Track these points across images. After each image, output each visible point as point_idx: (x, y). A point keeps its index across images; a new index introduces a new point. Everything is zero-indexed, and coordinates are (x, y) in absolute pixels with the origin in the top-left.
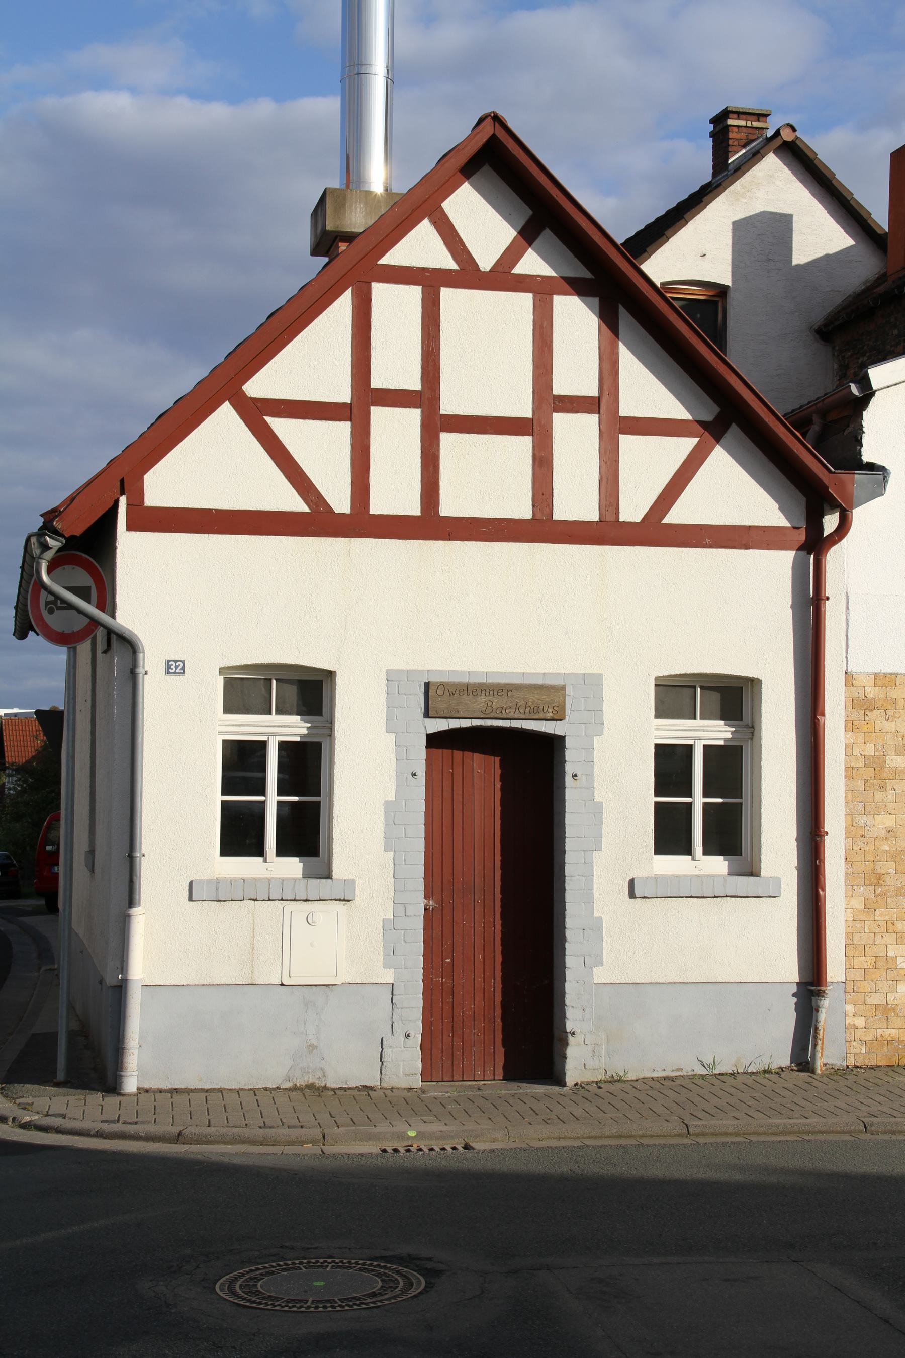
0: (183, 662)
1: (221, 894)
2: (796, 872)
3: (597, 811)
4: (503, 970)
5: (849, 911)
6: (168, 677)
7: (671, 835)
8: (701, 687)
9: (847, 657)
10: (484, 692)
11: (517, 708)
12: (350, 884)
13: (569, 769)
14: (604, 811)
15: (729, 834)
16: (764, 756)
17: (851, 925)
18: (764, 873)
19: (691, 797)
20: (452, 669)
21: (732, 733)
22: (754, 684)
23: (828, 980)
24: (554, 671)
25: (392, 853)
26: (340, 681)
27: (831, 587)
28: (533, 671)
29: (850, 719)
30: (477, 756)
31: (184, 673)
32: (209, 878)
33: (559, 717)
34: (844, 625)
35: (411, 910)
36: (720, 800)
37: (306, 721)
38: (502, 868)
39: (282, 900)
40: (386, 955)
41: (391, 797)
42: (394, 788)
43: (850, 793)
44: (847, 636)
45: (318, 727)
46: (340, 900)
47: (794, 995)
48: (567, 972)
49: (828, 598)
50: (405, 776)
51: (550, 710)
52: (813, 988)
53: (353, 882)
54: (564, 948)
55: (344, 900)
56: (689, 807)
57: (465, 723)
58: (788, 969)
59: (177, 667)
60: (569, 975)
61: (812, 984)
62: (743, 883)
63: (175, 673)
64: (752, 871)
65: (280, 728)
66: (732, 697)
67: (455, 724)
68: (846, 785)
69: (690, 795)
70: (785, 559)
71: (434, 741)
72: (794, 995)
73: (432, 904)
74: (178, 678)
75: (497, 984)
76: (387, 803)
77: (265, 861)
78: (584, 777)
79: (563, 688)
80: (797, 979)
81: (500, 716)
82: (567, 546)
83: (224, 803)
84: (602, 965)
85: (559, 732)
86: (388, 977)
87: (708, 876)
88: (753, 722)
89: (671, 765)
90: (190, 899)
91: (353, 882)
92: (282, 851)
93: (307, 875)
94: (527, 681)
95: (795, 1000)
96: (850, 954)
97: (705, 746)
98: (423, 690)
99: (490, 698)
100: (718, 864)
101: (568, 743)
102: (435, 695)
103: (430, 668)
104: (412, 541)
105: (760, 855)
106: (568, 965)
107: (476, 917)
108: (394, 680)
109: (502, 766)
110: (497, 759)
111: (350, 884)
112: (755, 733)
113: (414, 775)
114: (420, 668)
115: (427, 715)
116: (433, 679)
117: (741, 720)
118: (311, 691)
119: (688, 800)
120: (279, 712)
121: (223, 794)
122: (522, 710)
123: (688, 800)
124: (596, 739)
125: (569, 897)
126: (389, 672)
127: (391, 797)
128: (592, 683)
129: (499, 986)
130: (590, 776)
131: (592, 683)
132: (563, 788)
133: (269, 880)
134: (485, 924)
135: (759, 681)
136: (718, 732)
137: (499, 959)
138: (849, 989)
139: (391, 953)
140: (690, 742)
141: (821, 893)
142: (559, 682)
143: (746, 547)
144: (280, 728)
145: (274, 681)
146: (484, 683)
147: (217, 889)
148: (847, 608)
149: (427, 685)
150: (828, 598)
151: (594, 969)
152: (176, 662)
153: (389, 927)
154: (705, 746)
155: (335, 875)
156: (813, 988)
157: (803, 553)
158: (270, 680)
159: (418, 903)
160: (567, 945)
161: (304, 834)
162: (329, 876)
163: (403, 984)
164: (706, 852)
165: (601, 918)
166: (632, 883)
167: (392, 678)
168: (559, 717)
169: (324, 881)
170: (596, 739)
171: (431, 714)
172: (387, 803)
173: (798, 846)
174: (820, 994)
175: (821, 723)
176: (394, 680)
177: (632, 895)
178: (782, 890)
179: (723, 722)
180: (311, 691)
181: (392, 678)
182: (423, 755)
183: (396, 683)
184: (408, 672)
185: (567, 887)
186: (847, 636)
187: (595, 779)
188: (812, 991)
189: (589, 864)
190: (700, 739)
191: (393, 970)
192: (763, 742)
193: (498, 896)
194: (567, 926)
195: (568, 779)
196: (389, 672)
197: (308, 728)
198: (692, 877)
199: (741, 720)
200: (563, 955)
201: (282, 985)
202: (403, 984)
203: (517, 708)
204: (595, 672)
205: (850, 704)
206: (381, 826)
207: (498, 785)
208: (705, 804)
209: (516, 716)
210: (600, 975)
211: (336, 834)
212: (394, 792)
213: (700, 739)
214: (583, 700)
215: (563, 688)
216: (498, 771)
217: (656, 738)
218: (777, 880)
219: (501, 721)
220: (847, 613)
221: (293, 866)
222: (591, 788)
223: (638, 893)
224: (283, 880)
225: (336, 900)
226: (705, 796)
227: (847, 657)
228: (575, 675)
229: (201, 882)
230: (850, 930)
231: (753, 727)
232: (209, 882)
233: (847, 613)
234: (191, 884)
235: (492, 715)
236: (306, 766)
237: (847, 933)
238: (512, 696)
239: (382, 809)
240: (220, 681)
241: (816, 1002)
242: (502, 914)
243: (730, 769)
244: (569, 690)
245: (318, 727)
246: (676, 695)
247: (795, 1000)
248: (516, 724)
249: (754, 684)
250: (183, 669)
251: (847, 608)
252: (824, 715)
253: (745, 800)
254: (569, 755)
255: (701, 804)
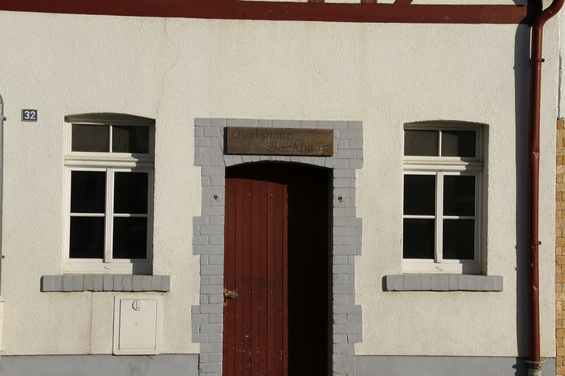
0: (36, 111)
1: (65, 285)
2: (515, 273)
3: (358, 225)
4: (289, 344)
5: (559, 303)
6: (25, 123)
7: (417, 243)
8: (443, 132)
9: (559, 107)
10: (269, 135)
11: (296, 147)
12: (166, 279)
13: (336, 193)
14: (364, 225)
15: (465, 243)
16: (490, 184)
17: (560, 313)
18: (489, 273)
19: (434, 215)
20: (245, 118)
21: (466, 166)
22: (483, 128)
23: (542, 355)
24: (325, 119)
25: (199, 256)
26: (158, 126)
27: (545, 53)
28: (309, 120)
29: (561, 154)
30: (270, 184)
31: (36, 120)
32: (57, 274)
33: (328, 153)
34: (557, 81)
35: (213, 299)
36: (128, 215)
37: (135, 157)
38: (289, 267)
39: (113, 291)
40: (194, 332)
41: (199, 214)
42: (200, 207)
43: (560, 212)
44: (559, 90)
45: (144, 162)
46: (158, 291)
47: (514, 367)
48: (334, 347)
49: (543, 60)
50: (208, 198)
51: (321, 149)
52: (529, 362)
53: (168, 277)
54: (332, 329)
55: (161, 291)
56: (432, 222)
57: (256, 159)
58: (510, 347)
59: (31, 115)
60: (336, 349)
61: (528, 359)
62: (473, 280)
63: (29, 120)
64: (482, 272)
65: (115, 162)
66: (467, 139)
67: (248, 159)
68: (557, 206)
69: (103, 211)
70: (509, 31)
71: (232, 173)
72: (514, 367)
73: (232, 293)
74: (32, 123)
75: (284, 354)
76: (195, 219)
77: (104, 262)
78: (348, 199)
79: (331, 132)
80: (516, 354)
81: (282, 153)
82: (336, 23)
83: (72, 218)
84: (361, 341)
85: (328, 165)
86: (196, 349)
87: (446, 274)
88: (483, 157)
89: (417, 191)
90: (42, 290)
91: (168, 277)
92: (117, 254)
93: (136, 272)
94: (303, 127)
95: (515, 370)
96: (560, 335)
97: (445, 176)
98: (223, 134)
99: (275, 140)
100: (455, 266)
101: (336, 173)
102: (235, 137)
103: (229, 117)
104: (214, 20)
105: (486, 259)
106: (334, 341)
107: (269, 304)
108: (201, 126)
109: (289, 191)
110: (285, 187)
111: (166, 279)
112: (485, 166)
113: (216, 197)
114: (221, 117)
115: (226, 152)
116: (230, 125)
117: (474, 156)
118: (136, 134)
119: (432, 217)
120: (115, 150)
121: (405, 214)
122: (299, 149)
123: (432, 217)
124: (357, 171)
125: (336, 289)
126: (196, 120)
127: (199, 214)
128: (355, 129)
129: (286, 356)
130: (352, 199)
131: (355, 129)
132: (332, 207)
133: (103, 276)
134: (276, 309)
135: (488, 126)
136: (456, 165)
137: (286, 335)
138: (560, 363)
139: (198, 333)
140: (434, 173)
141: (535, 288)
142: (329, 127)
143: (478, 21)
144: (115, 162)
145: (111, 127)
146: (269, 128)
147: (62, 283)
148: (560, 68)
149: (226, 130)
150: (543, 60)
151: (355, 345)
152: (30, 111)
153: (196, 311)
154: (445, 176)
155: (155, 273)
156: (529, 362)
157: (524, 26)
158: (108, 127)
159: (218, 292)
160: (334, 326)
161: (135, 242)
162: (151, 274)
163: (207, 355)
164: (445, 257)
165: (360, 306)
166: (384, 279)
167: (199, 124)
168: (328, 153)
169: (145, 277)
170: (357, 171)
171: (228, 151)
172: (195, 219)
173: (517, 253)
174: (535, 367)
175: (536, 157)
176: (201, 126)
177: (385, 289)
178: (504, 286)
179: (459, 158)
180: (136, 134)
181: (199, 124)
182: (223, 183)
183: (202, 128)
184: (211, 120)
185: (334, 282)
186: (559, 90)
187: (357, 201)
188: (528, 364)
189: (351, 265)
190: (441, 171)
191: (199, 344)
192: (490, 173)
193: (286, 288)
194: (334, 312)
195: (336, 202)
196: (196, 120)
197: (137, 163)
198: (431, 276)
199: (474, 156)
200: (332, 334)
201: (113, 355)
202: (207, 355)
203: (296, 147)
204: (357, 120)
205: (561, 143)
206: (190, 235)
207: (286, 206)
208: (445, 220)
209: (294, 153)
210: (360, 349)
211: (155, 243)
212: (200, 210)
213: (441, 171)
214: (347, 141)
215: (331, 132)
216: (286, 195)
217: (405, 170)
218: (500, 279)
219: (283, 157)
220: (560, 72)
221: (125, 266)
222: (353, 208)
223: (389, 287)
224: (114, 276)
225: (155, 291)
226: (445, 214)
227: (559, 107)
228: (342, 122)
229: (50, 277)
230: (560, 317)
231: (483, 162)
232: (56, 277)
233: (560, 72)
234: (42, 279)
235: (276, 152)
236: (136, 191)
237: (557, 321)
238: (292, 138)
239: (192, 222)
240: (68, 128)
241: (532, 373)
242: (289, 302)
243: (466, 193)
244: (336, 134)
245: (144, 162)
246: (421, 137)
247: (515, 370)
248: (274, 158)
249: (483, 128)
250: (36, 116)
251: (560, 68)
252: (538, 151)
253: (477, 218)
254: (336, 183)
255: (444, 221)
